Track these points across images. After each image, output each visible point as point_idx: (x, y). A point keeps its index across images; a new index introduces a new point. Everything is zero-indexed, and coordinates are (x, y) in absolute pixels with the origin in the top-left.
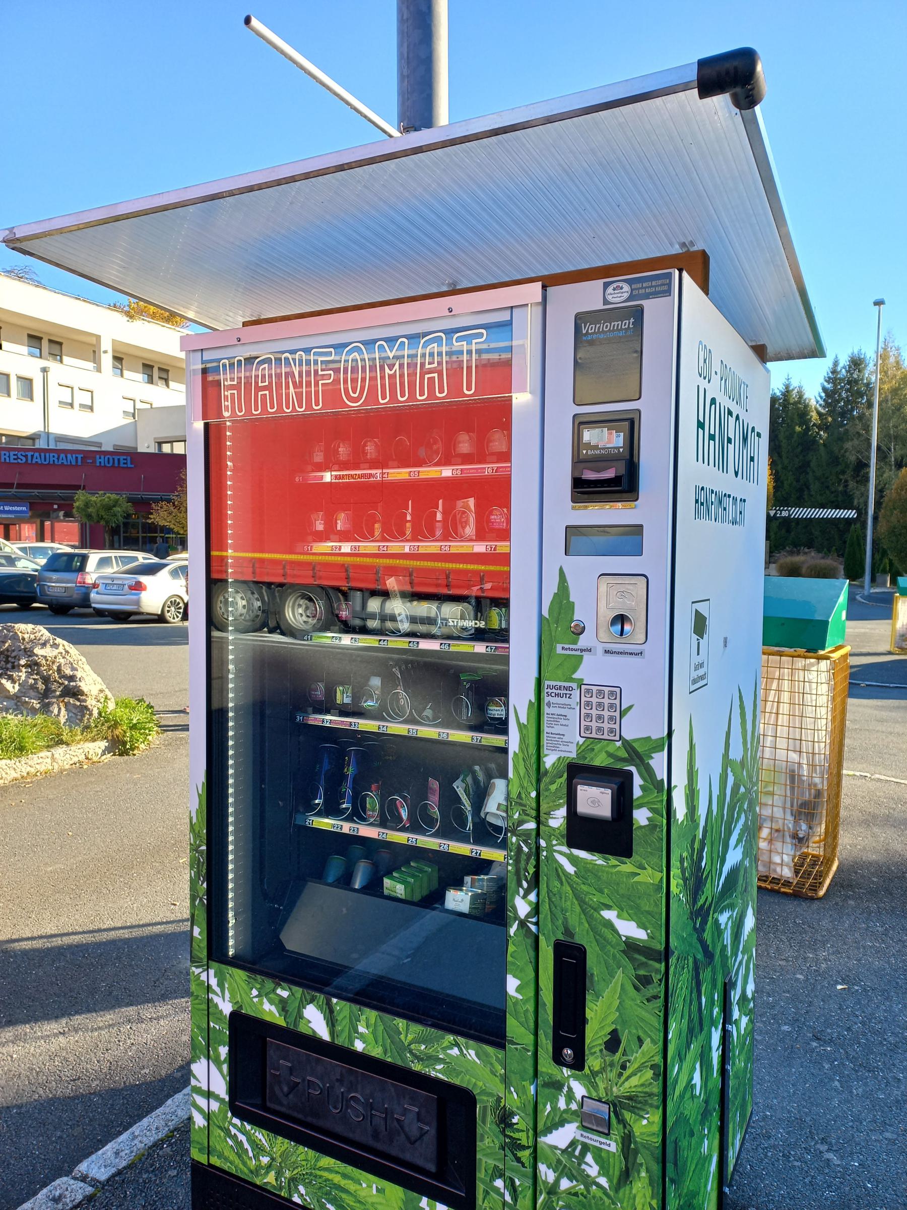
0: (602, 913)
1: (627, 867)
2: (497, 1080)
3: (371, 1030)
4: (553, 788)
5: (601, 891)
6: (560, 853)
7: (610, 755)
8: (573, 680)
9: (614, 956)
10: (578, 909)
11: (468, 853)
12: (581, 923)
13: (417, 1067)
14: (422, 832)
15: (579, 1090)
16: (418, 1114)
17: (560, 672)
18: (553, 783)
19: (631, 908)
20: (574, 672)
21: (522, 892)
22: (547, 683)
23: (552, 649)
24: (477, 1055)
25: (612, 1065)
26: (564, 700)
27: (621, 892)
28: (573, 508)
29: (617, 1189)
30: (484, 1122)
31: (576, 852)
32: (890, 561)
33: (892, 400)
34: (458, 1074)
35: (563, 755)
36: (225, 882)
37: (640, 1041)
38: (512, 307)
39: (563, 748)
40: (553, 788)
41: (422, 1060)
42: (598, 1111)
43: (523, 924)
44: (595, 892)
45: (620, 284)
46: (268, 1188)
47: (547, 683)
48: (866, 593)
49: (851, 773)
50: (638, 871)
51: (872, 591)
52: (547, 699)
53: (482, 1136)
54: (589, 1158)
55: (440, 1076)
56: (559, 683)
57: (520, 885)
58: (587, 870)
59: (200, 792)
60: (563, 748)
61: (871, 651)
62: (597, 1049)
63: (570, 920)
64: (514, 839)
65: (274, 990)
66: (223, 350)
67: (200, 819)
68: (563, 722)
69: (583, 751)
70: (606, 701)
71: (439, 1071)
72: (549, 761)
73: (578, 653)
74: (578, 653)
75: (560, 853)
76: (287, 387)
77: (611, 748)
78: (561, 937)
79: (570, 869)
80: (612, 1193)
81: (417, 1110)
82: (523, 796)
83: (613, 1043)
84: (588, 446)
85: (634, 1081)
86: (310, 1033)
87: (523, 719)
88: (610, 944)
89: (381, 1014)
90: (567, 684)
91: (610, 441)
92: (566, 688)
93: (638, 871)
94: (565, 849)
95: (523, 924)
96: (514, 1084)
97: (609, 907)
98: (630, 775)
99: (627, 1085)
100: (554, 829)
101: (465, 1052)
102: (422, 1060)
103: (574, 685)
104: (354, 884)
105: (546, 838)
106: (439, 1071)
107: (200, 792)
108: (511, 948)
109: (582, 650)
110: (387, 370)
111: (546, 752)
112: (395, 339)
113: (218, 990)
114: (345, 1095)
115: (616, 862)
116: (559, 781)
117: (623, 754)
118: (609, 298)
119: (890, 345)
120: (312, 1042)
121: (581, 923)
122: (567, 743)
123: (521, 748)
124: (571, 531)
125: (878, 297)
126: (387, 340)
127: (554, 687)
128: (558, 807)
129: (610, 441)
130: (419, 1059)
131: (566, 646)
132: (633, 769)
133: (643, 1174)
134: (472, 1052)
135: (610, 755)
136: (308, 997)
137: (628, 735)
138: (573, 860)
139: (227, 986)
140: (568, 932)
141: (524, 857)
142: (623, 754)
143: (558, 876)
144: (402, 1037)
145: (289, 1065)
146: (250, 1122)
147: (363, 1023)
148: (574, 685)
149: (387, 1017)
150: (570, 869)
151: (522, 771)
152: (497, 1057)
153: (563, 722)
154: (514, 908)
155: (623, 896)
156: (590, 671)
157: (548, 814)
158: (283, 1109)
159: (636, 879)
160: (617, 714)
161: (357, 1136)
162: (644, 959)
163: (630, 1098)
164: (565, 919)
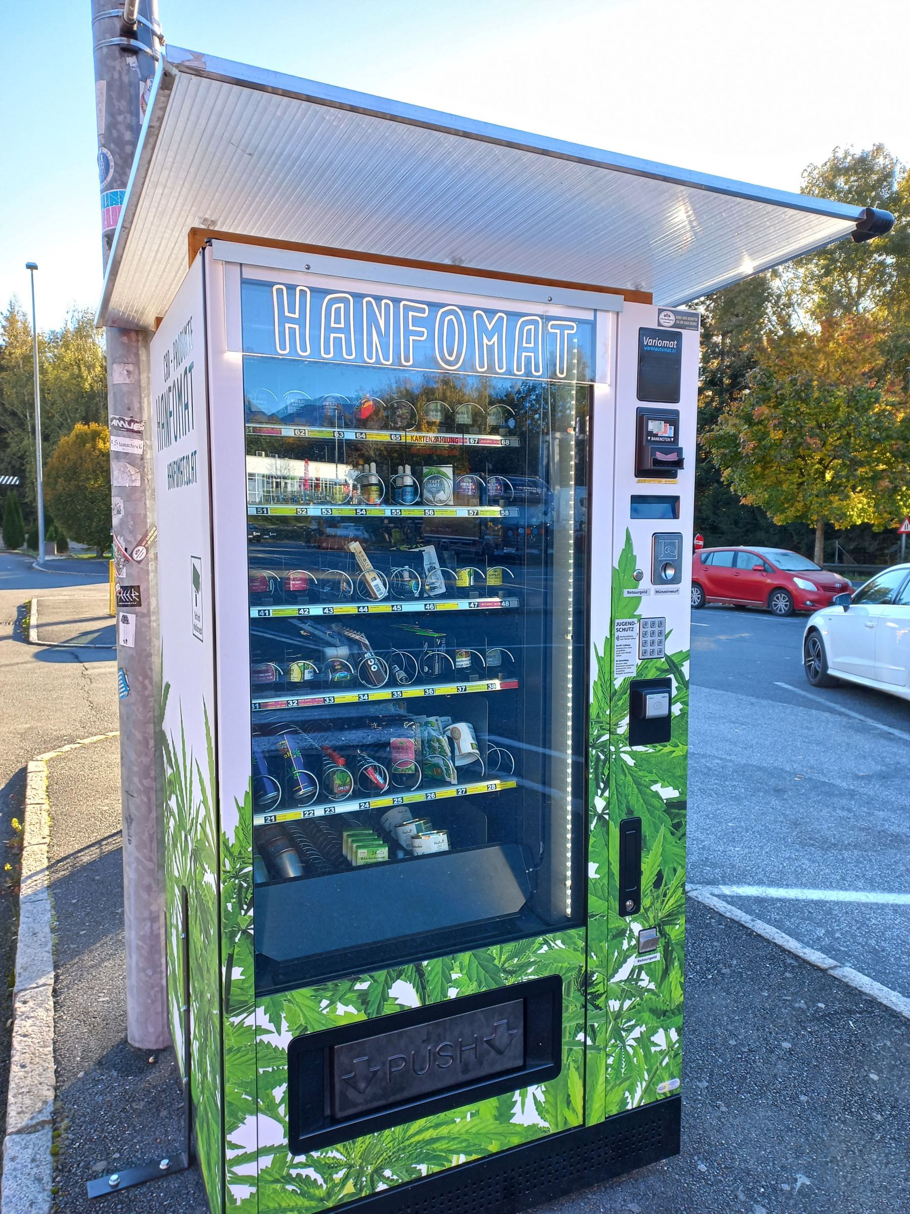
0: (652, 788)
1: (668, 749)
2: (579, 953)
3: (464, 972)
4: (620, 703)
5: (651, 772)
6: (624, 752)
7: (658, 669)
8: (635, 616)
9: (659, 817)
10: (636, 791)
11: (455, 794)
12: (638, 801)
13: (511, 981)
14: (408, 789)
15: (636, 927)
16: (508, 1023)
17: (626, 611)
18: (619, 700)
19: (670, 777)
20: (635, 611)
21: (599, 792)
22: (617, 621)
23: (621, 593)
24: (563, 943)
25: (658, 897)
26: (629, 633)
27: (664, 768)
28: (638, 482)
29: (659, 986)
30: (568, 995)
31: (635, 748)
32: (55, 527)
33: (24, 367)
34: (546, 966)
35: (627, 676)
36: (574, 831)
37: (675, 870)
38: (595, 310)
39: (627, 670)
40: (620, 703)
41: (515, 972)
42: (650, 936)
43: (600, 817)
44: (647, 774)
45: (669, 313)
46: (345, 1201)
47: (617, 621)
48: (41, 561)
49: (111, 734)
50: (673, 749)
51: (47, 558)
52: (617, 634)
53: (567, 1007)
54: (643, 975)
55: (532, 977)
56: (625, 620)
57: (598, 787)
58: (642, 759)
59: (242, 804)
60: (627, 670)
61: (95, 616)
62: (648, 891)
63: (631, 802)
64: (594, 752)
65: (351, 990)
66: (276, 273)
67: (241, 836)
68: (627, 650)
69: (641, 670)
70: (649, 630)
71: (531, 974)
72: (618, 683)
73: (638, 595)
74: (638, 595)
75: (624, 752)
76: (370, 334)
77: (658, 664)
78: (624, 817)
79: (631, 762)
80: (656, 991)
81: (506, 1021)
82: (601, 715)
83: (658, 883)
84: (651, 434)
85: (672, 901)
86: (398, 1009)
87: (601, 654)
88: (656, 809)
89: (474, 951)
90: (630, 620)
91: (665, 432)
92: (630, 623)
93: (673, 749)
94: (628, 749)
95: (600, 817)
96: (594, 949)
97: (655, 782)
98: (670, 679)
99: (667, 906)
100: (620, 735)
101: (553, 945)
102: (515, 972)
103: (635, 620)
104: (287, 873)
105: (615, 744)
106: (531, 974)
107: (242, 804)
108: (592, 840)
109: (641, 593)
110: (485, 341)
111: (616, 676)
112: (495, 312)
113: (271, 1027)
114: (432, 1051)
115: (659, 747)
116: (624, 697)
117: (666, 667)
118: (662, 321)
119: (16, 309)
120: (407, 1017)
121: (638, 801)
122: (630, 666)
123: (599, 677)
124: (637, 500)
125: (32, 260)
126: (486, 311)
127: (622, 624)
128: (623, 717)
129: (665, 432)
130: (511, 973)
131: (630, 590)
132: (672, 676)
133: (676, 964)
134: (559, 942)
135: (658, 669)
136: (394, 975)
137: (669, 653)
138: (633, 755)
139: (283, 1015)
140: (630, 811)
141: (601, 763)
142: (666, 667)
143: (623, 770)
144: (496, 962)
145: (366, 1058)
146: (316, 1148)
147: (457, 969)
148: (635, 620)
149: (480, 951)
150: (631, 762)
151: (600, 695)
152: (578, 935)
153: (627, 650)
154: (594, 807)
155: (665, 771)
156: (646, 609)
157: (617, 724)
158: (364, 1108)
159: (673, 755)
160: (663, 638)
161: (451, 1081)
162: (677, 811)
163: (669, 915)
164: (628, 802)
